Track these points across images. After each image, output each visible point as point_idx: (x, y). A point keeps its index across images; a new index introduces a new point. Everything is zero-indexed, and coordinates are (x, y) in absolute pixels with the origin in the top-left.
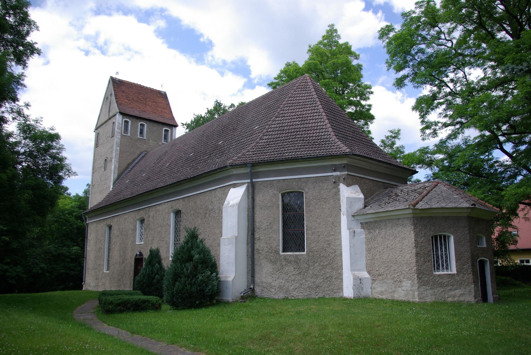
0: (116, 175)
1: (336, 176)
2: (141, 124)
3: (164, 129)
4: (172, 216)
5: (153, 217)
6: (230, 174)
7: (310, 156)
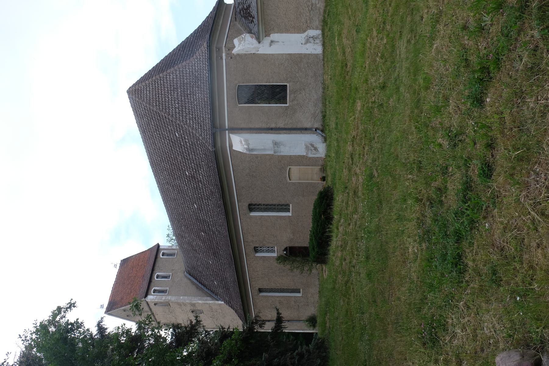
0: (209, 298)
1: (226, 56)
2: (157, 278)
4: (253, 214)
5: (253, 236)
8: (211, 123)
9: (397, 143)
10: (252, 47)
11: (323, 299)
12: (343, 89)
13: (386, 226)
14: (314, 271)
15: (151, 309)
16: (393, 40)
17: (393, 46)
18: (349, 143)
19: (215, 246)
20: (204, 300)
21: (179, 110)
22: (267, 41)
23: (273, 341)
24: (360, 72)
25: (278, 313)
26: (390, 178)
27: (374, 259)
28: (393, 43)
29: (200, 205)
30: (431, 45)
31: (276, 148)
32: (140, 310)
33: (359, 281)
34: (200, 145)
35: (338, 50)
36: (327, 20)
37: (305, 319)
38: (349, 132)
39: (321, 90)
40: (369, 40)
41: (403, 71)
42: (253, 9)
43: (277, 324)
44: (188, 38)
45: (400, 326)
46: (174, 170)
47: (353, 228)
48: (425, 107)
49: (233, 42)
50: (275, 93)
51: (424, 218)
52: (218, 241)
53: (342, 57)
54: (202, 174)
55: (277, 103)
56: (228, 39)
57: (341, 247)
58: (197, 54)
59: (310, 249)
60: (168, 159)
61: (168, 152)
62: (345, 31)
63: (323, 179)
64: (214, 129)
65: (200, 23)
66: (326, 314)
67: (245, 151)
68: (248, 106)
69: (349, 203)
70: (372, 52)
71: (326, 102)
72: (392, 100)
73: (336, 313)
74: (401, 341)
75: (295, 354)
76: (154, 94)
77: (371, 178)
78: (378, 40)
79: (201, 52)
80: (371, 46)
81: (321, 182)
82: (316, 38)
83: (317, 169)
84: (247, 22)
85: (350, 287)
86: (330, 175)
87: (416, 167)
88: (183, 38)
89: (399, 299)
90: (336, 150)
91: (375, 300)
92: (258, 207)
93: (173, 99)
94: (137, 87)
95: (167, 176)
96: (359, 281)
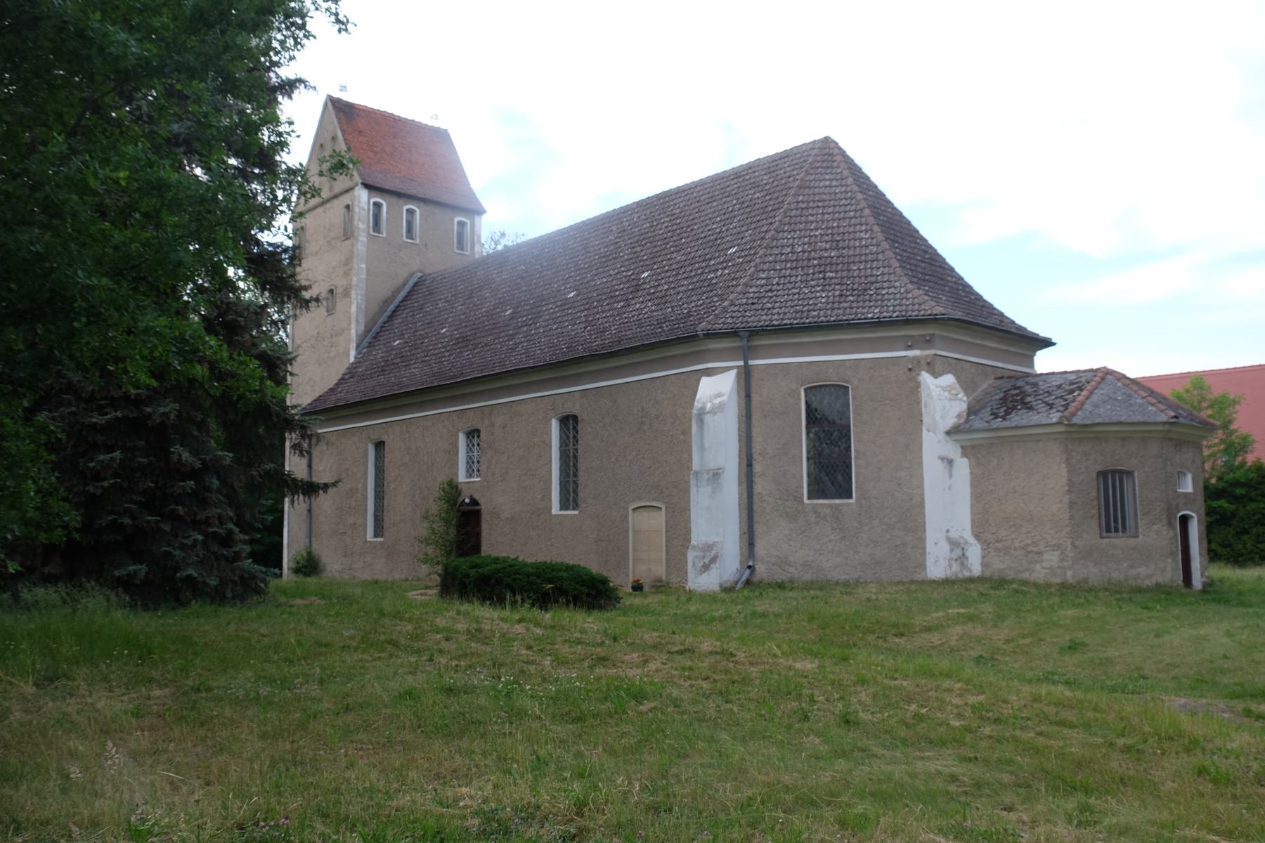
0: (362, 327)
1: (914, 358)
3: (405, 208)
4: (555, 425)
6: (702, 348)
7: (865, 319)
8: (761, 326)
9: (716, 754)
10: (937, 417)
11: (358, 591)
12: (844, 628)
13: (522, 732)
14: (425, 569)
15: (336, 197)
16: (956, 741)
17: (943, 743)
18: (718, 643)
19: (482, 340)
20: (357, 316)
21: (788, 254)
22: (952, 450)
23: (260, 476)
24: (882, 666)
25: (326, 487)
26: (633, 741)
27: (446, 707)
28: (951, 742)
29: (576, 304)
30: (945, 830)
31: (706, 476)
32: (331, 173)
33: (396, 673)
34: (710, 303)
35: (935, 615)
36: (1005, 589)
37: (313, 549)
38: (744, 644)
39: (843, 578)
40: (958, 685)
41: (882, 766)
42: (1024, 417)
43: (300, 484)
44: (952, 270)
45: (287, 769)
46: (654, 244)
47: (521, 658)
48: (797, 820)
49: (947, 373)
50: (832, 472)
51: (540, 822)
52: (492, 347)
53: (920, 624)
54: (645, 308)
55: (809, 475)
56: (954, 361)
57: (476, 630)
58: (916, 292)
59: (475, 559)
60: (678, 231)
61: (692, 230)
62: (979, 631)
63: (637, 587)
64: (747, 334)
65: (988, 297)
66: (323, 597)
67: (697, 405)
68: (800, 410)
69: (579, 647)
70: (930, 693)
71: (814, 589)
72: (817, 741)
73: (325, 621)
74: (252, 771)
75: (231, 526)
76: (824, 197)
77: (635, 697)
78: (957, 707)
79: (920, 300)
80: (944, 690)
81: (631, 581)
82: (962, 564)
83: (660, 571)
84: (993, 403)
85: (383, 650)
86: (646, 602)
87: (659, 800)
88: (951, 260)
89: (351, 766)
90: (704, 614)
91: (351, 710)
92: (571, 436)
93: (813, 239)
94: (839, 158)
95: (639, 231)
96: (396, 673)
